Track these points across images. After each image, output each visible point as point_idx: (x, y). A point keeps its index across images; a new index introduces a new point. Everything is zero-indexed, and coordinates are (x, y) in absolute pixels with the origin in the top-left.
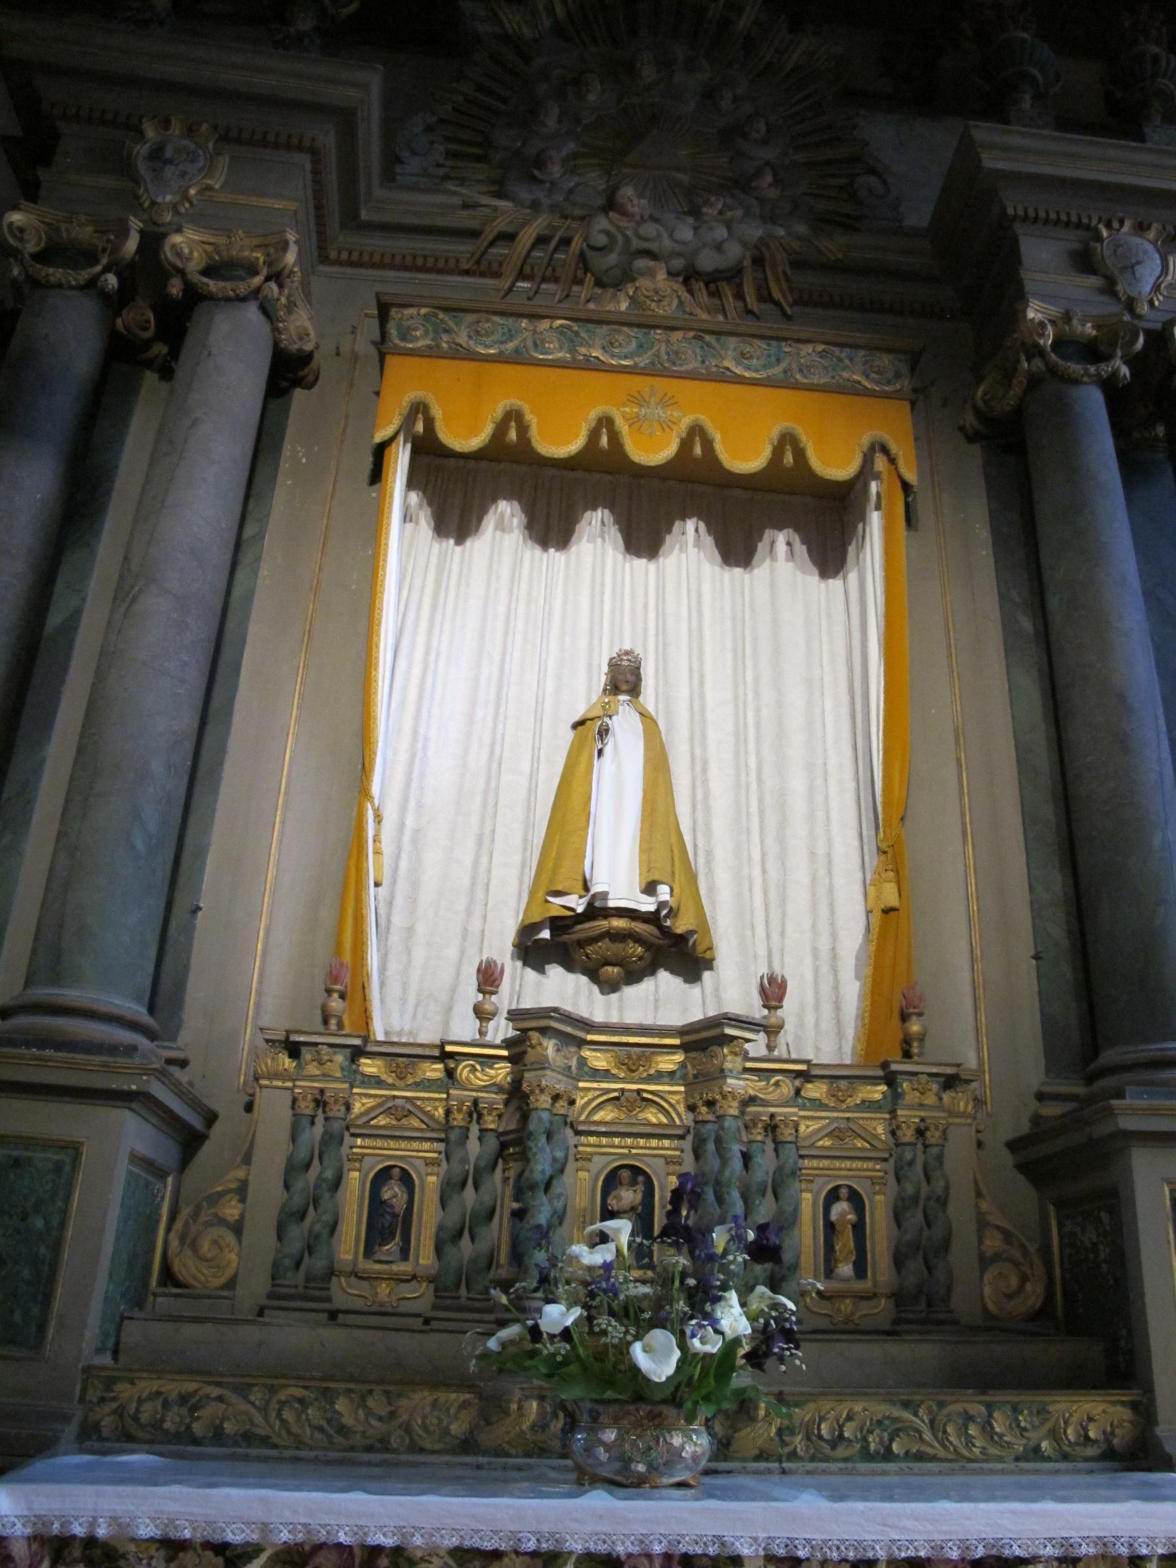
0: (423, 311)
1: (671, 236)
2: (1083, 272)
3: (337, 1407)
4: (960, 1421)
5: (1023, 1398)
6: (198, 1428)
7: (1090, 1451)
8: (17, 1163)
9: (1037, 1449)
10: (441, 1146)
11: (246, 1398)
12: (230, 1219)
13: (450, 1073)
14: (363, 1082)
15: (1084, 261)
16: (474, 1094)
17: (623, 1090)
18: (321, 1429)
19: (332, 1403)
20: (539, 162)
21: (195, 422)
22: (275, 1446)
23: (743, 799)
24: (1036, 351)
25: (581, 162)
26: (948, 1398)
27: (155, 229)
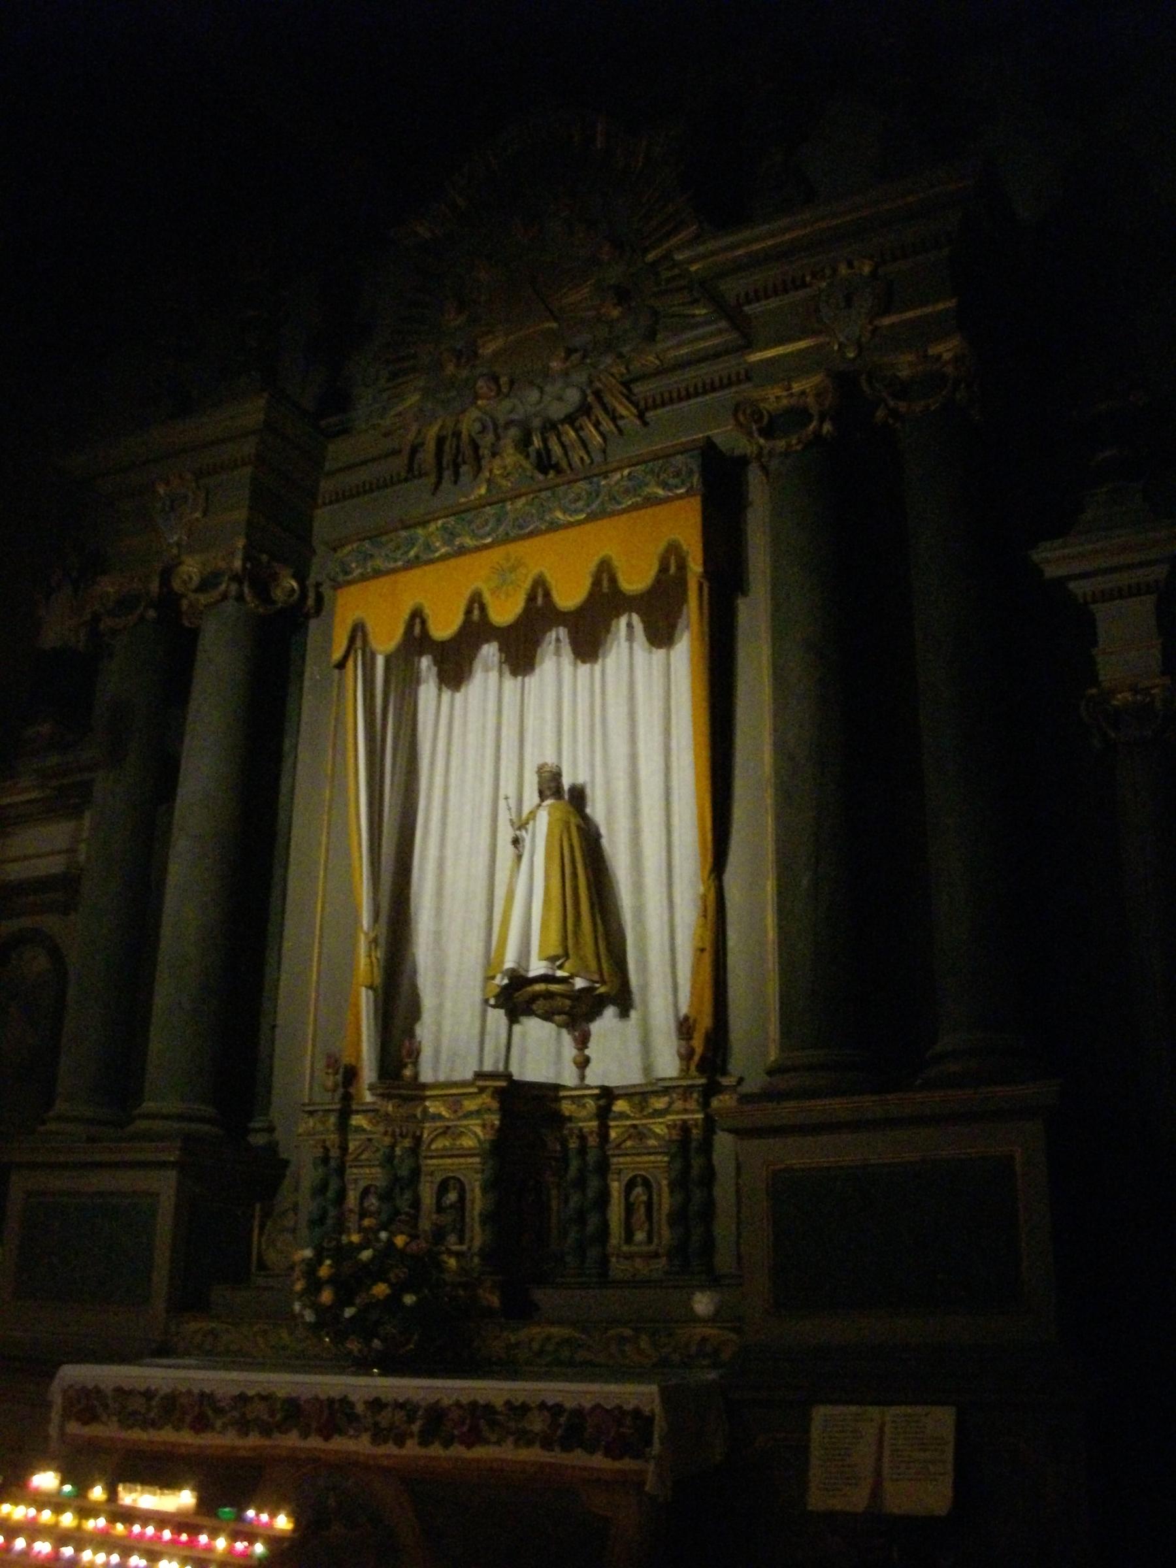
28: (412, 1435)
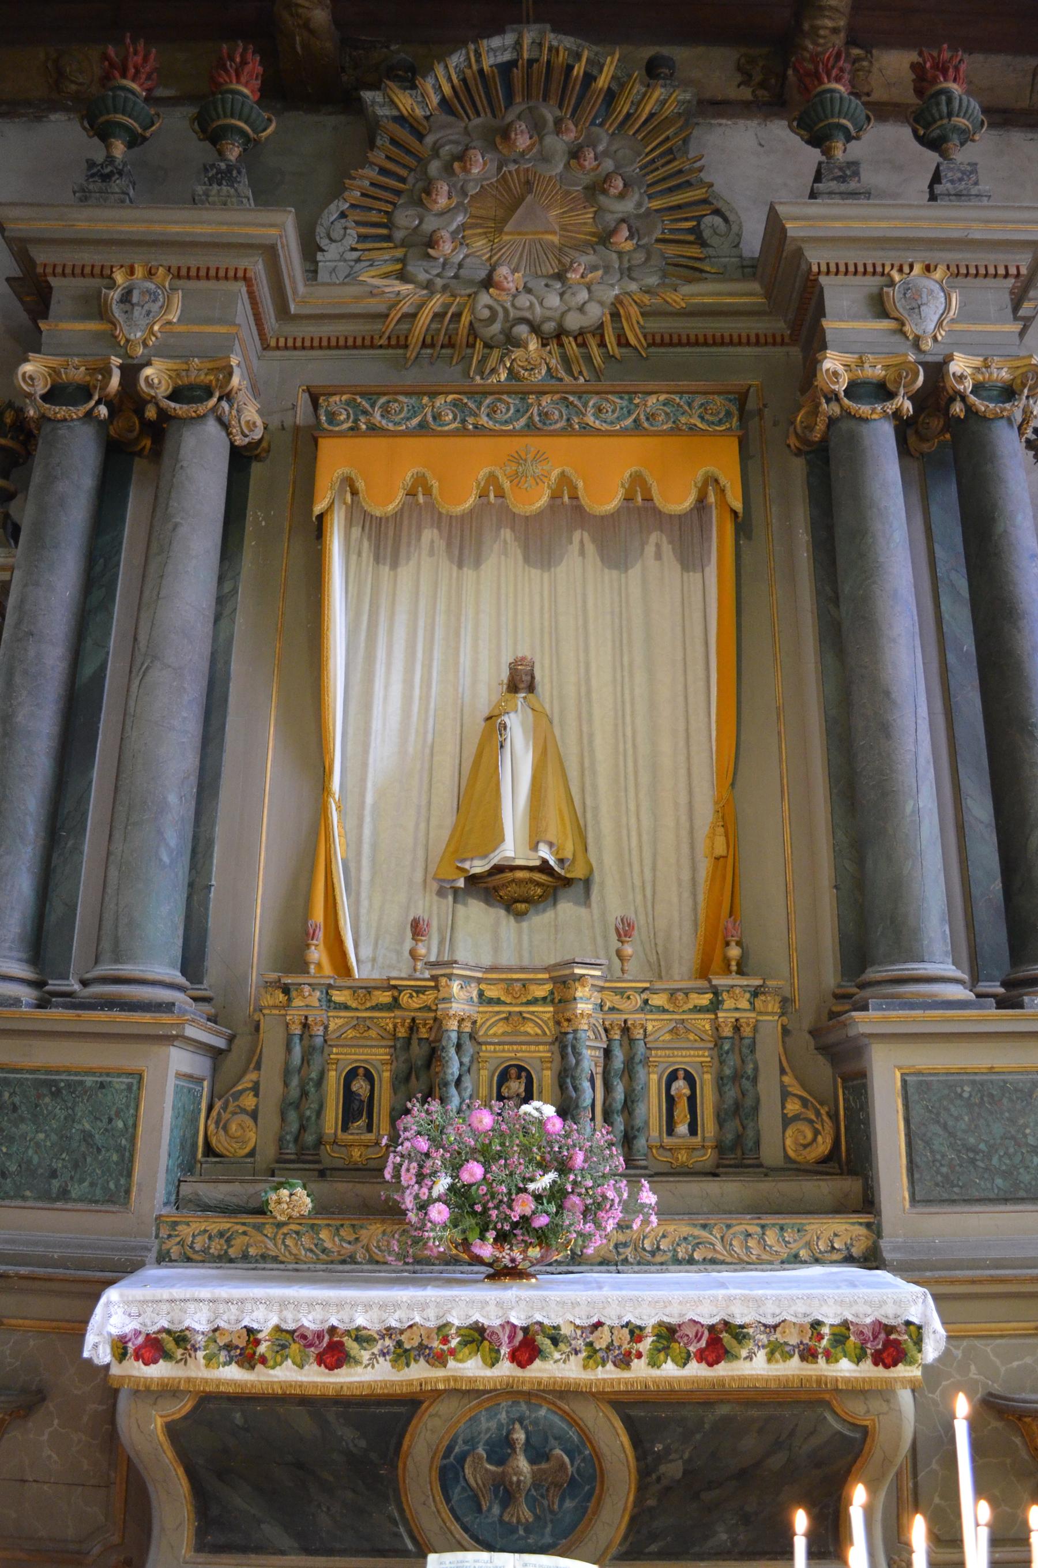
0: (344, 397)
1: (541, 303)
2: (879, 317)
3: (321, 1236)
4: (742, 1237)
5: (787, 1221)
6: (232, 1252)
7: (836, 1256)
8: (102, 1086)
9: (796, 1256)
10: (392, 1050)
11: (261, 1232)
12: (249, 1109)
13: (395, 999)
14: (335, 1008)
15: (879, 307)
16: (412, 1014)
17: (510, 1013)
18: (311, 1251)
19: (318, 1234)
20: (431, 242)
21: (176, 526)
22: (282, 1262)
23: (621, 763)
24: (833, 397)
25: (468, 232)
26: (734, 1222)
27: (130, 361)
28: (639, 1355)
